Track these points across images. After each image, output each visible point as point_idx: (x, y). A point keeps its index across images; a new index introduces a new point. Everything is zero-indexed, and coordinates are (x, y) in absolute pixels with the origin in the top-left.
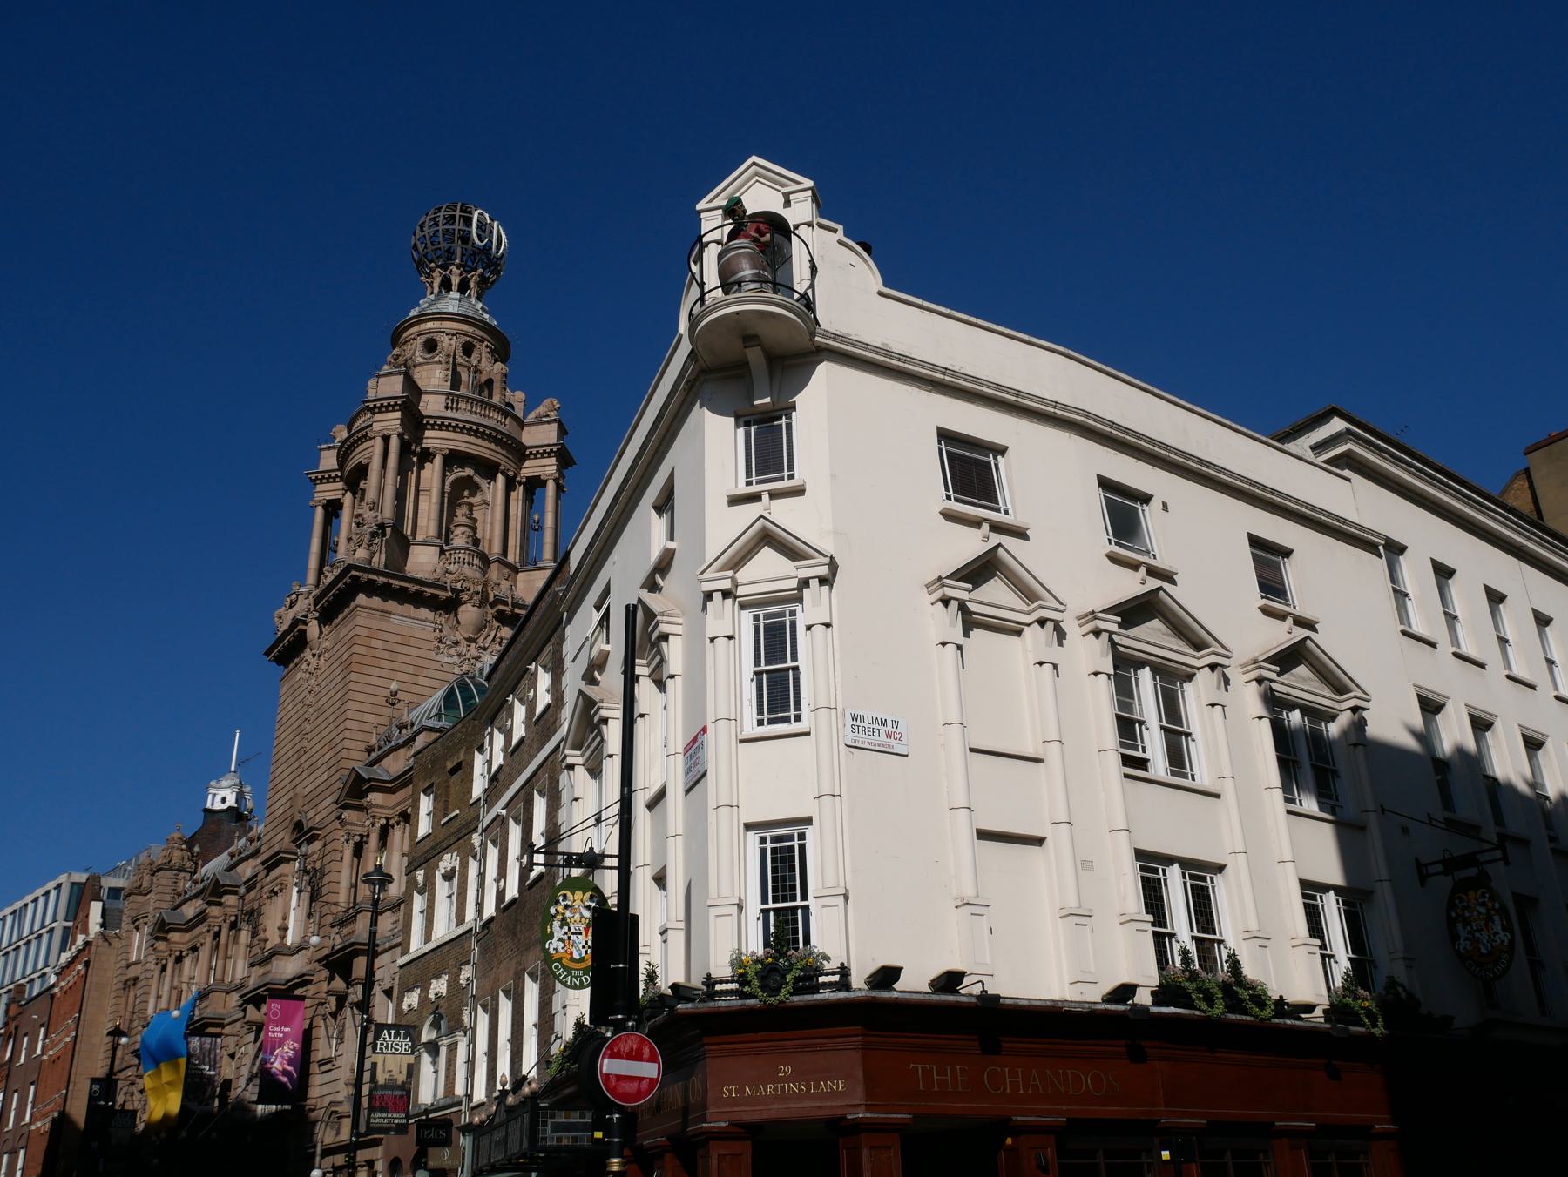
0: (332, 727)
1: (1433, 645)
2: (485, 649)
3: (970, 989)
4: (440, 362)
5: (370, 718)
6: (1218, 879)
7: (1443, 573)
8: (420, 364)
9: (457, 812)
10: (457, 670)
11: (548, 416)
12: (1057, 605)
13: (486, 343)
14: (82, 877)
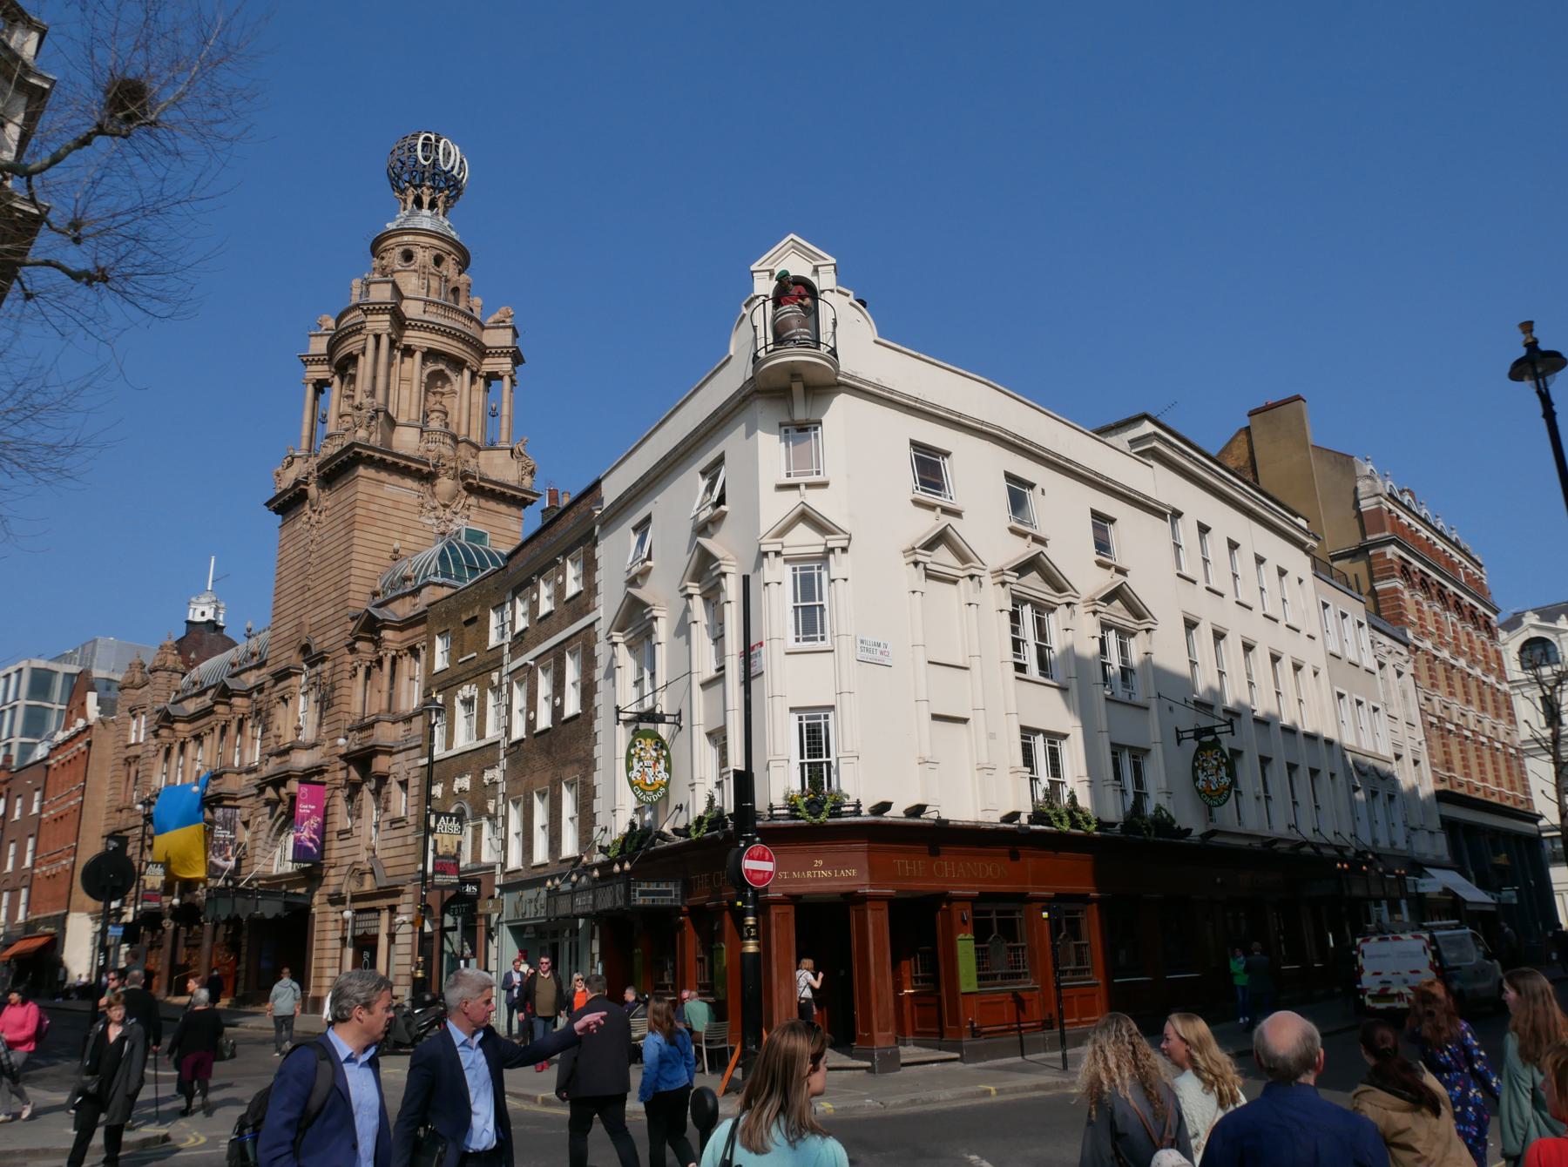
0: (336, 572)
1: (1194, 582)
2: (456, 513)
3: (930, 815)
4: (415, 271)
5: (369, 567)
6: (1064, 743)
7: (1204, 529)
8: (399, 271)
9: (475, 654)
10: (435, 530)
11: (504, 322)
12: (981, 566)
13: (453, 256)
14: (75, 669)
